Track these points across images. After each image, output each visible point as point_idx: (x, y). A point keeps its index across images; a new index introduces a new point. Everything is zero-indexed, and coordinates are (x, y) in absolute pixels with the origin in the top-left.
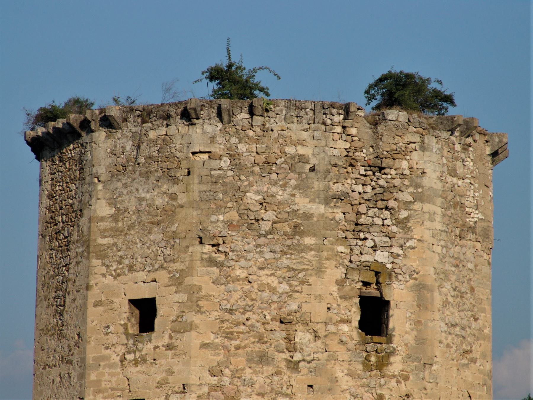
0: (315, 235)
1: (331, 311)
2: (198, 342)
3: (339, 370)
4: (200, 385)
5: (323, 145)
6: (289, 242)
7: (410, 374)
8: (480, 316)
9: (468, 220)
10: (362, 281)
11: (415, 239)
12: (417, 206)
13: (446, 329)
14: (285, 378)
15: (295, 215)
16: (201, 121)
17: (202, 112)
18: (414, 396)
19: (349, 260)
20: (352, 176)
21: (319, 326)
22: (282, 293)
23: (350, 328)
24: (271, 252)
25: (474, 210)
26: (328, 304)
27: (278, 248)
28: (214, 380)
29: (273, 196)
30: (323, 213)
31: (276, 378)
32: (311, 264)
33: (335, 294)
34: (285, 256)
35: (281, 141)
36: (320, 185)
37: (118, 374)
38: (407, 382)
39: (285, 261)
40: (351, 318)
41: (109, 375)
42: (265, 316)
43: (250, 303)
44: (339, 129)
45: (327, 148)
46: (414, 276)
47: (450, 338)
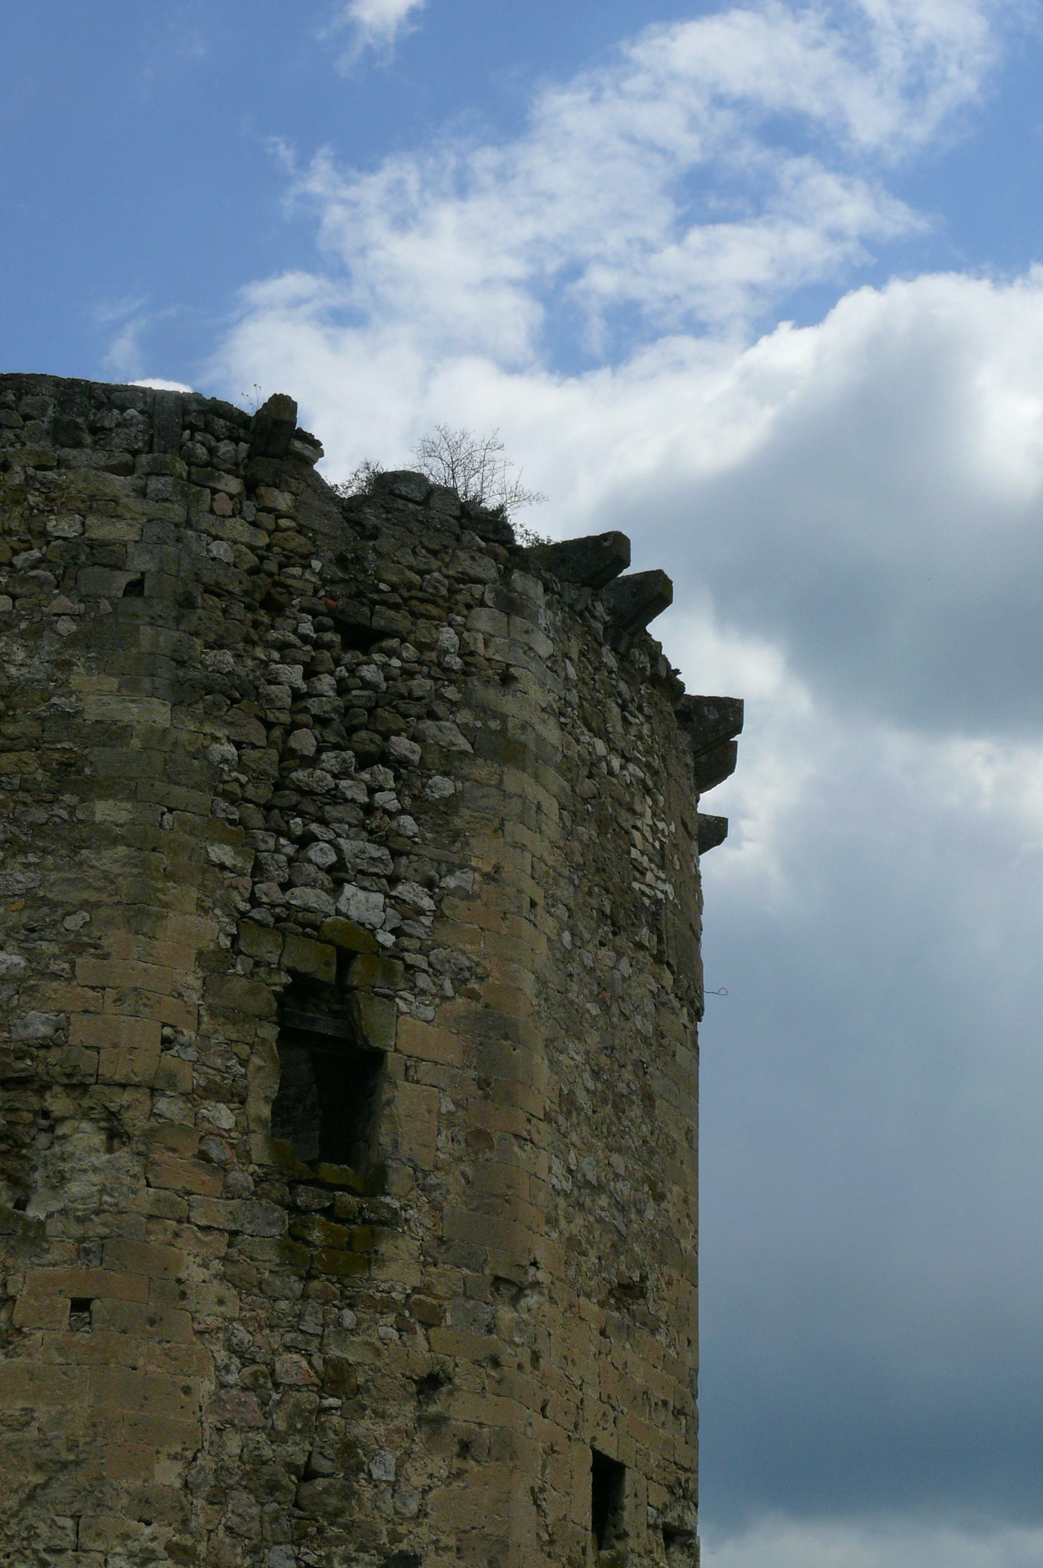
0: (133, 796)
1: (173, 1052)
3: (191, 1258)
5: (177, 520)
6: (39, 815)
8: (671, 1191)
9: (636, 885)
10: (291, 972)
11: (475, 870)
13: (567, 1186)
18: (457, 1381)
19: (247, 895)
23: (242, 1119)
25: (653, 866)
26: (164, 1025)
30: (165, 730)
32: (111, 888)
33: (194, 997)
34: (21, 859)
35: (33, 499)
36: (161, 639)
38: (432, 1332)
40: (246, 1087)
44: (233, 485)
46: (470, 986)
47: (579, 1221)
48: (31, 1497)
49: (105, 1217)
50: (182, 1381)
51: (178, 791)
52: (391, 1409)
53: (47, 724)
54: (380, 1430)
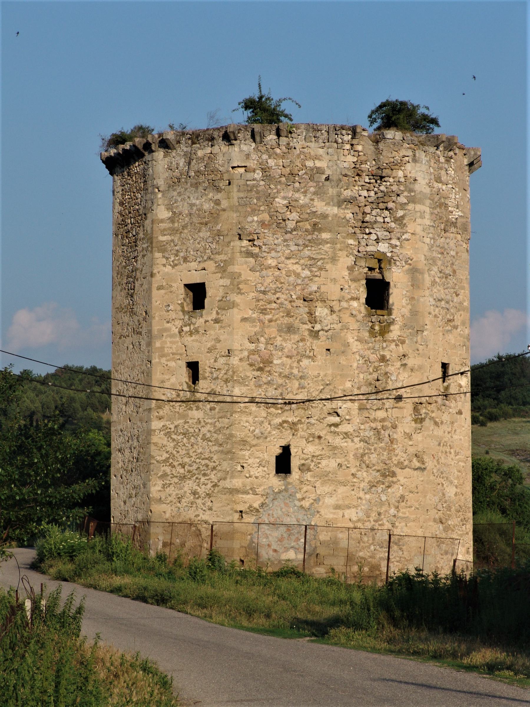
0: (330, 231)
4: (241, 350)
6: (309, 237)
9: (450, 217)
10: (367, 267)
14: (308, 344)
16: (238, 141)
17: (239, 135)
20: (359, 183)
21: (334, 303)
22: (305, 278)
27: (301, 242)
28: (252, 346)
31: (301, 344)
33: (347, 278)
34: (306, 248)
35: (302, 157)
37: (177, 342)
39: (307, 252)
42: (291, 296)
43: (280, 286)
44: (348, 147)
45: (339, 162)
47: (437, 310)
48: (321, 392)
49: (331, 331)
50: (350, 365)
51: (341, 228)
52: (395, 364)
53: (310, 215)
54: (393, 369)
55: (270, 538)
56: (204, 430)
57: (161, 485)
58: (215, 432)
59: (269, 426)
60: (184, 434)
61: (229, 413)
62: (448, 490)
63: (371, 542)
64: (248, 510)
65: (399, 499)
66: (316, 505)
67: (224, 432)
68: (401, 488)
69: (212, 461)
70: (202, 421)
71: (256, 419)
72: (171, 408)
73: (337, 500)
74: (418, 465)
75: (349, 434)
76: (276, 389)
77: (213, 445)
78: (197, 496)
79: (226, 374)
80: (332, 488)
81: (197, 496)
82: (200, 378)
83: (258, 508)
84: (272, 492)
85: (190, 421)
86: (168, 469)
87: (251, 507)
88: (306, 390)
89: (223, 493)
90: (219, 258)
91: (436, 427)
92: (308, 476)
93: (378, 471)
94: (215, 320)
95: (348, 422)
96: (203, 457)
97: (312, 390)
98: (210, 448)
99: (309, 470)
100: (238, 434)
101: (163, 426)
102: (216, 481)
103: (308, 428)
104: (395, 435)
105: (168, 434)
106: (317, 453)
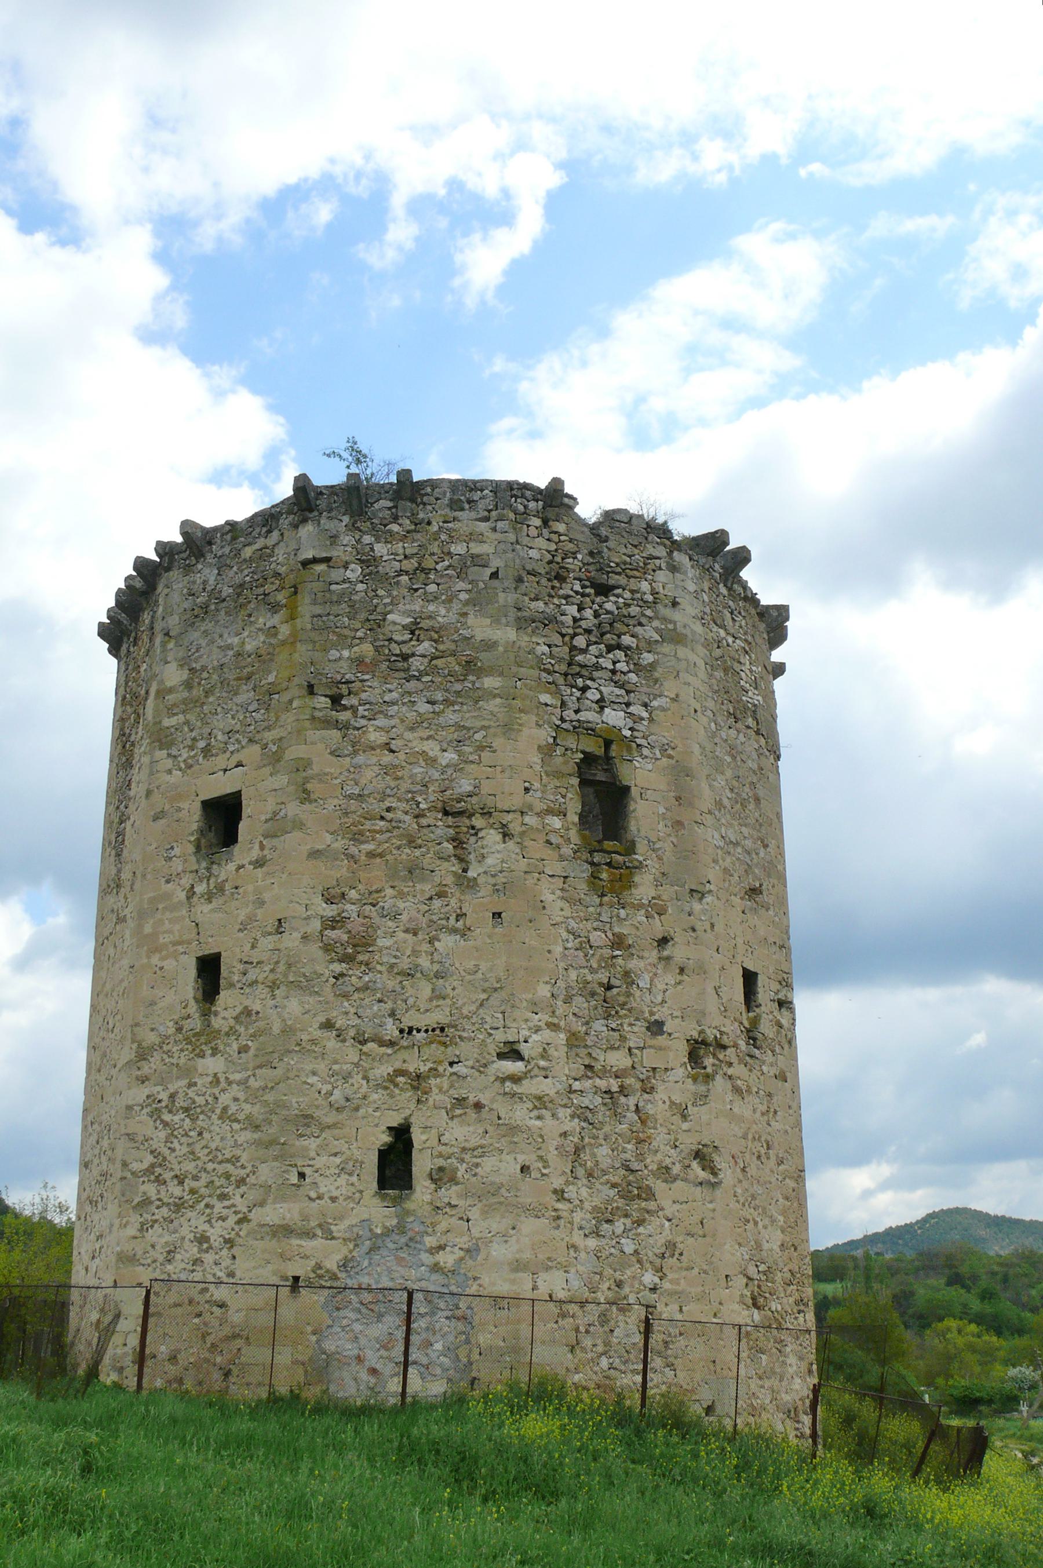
0: (501, 674)
2: (305, 848)
4: (308, 918)
6: (458, 687)
7: (668, 904)
9: (744, 698)
10: (582, 752)
12: (666, 648)
14: (453, 902)
15: (468, 644)
16: (316, 513)
17: (318, 502)
20: (561, 592)
21: (510, 816)
22: (447, 766)
24: (428, 702)
27: (439, 696)
28: (330, 911)
29: (430, 617)
31: (437, 903)
33: (538, 768)
34: (451, 708)
35: (443, 537)
37: (183, 918)
39: (451, 716)
41: (170, 923)
42: (418, 804)
43: (393, 784)
44: (537, 522)
45: (518, 547)
48: (481, 1005)
52: (646, 954)
54: (642, 964)
55: (363, 1341)
56: (225, 1099)
57: (138, 1226)
58: (246, 1101)
59: (364, 1082)
60: (186, 1110)
61: (276, 1055)
62: (765, 1234)
63: (600, 1349)
64: (312, 1275)
65: (663, 1249)
66: (470, 1263)
67: (265, 1098)
68: (667, 1224)
69: (239, 1164)
70: (222, 1080)
71: (336, 1067)
72: (165, 1056)
73: (520, 1251)
74: (703, 1175)
75: (546, 1099)
76: (380, 1001)
77: (241, 1129)
78: (205, 1246)
79: (272, 971)
80: (507, 1222)
81: (205, 1246)
82: (222, 987)
83: (335, 1268)
84: (369, 1234)
85: (200, 1082)
86: (151, 1190)
87: (320, 1268)
88: (448, 1001)
89: (259, 1237)
90: (269, 736)
91: (737, 1097)
92: (450, 1194)
93: (614, 1186)
94: (257, 861)
95: (544, 1073)
96: (220, 1157)
97: (460, 1002)
98: (236, 1137)
99: (453, 1180)
100: (294, 1100)
101: (148, 1097)
102: (245, 1210)
103: (452, 1086)
104: (649, 1106)
105: (155, 1114)
106: (474, 1142)
